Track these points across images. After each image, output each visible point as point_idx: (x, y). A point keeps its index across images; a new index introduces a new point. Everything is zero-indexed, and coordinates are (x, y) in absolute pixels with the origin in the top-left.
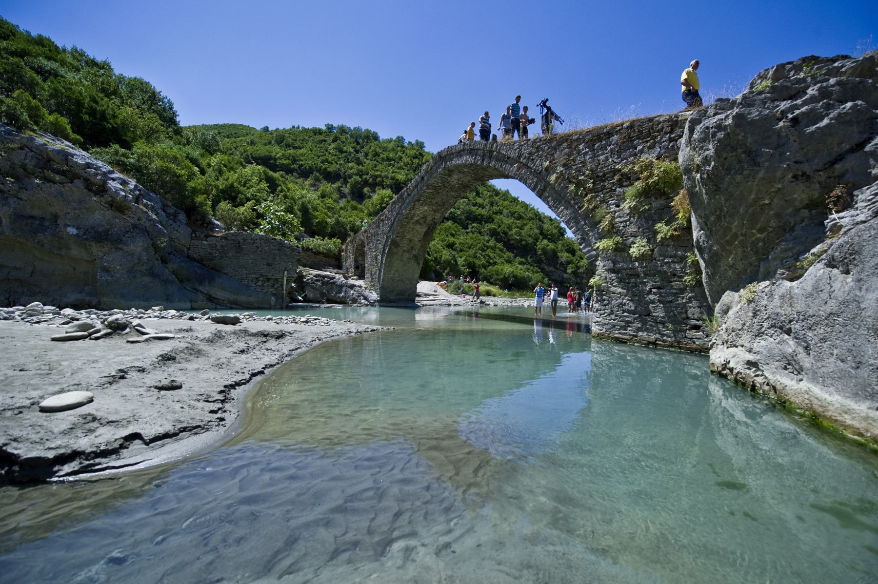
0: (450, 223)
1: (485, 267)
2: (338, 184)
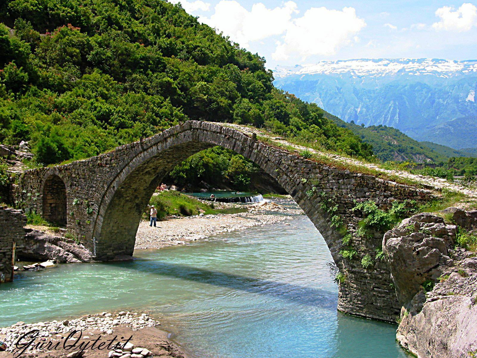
0: (96, 74)
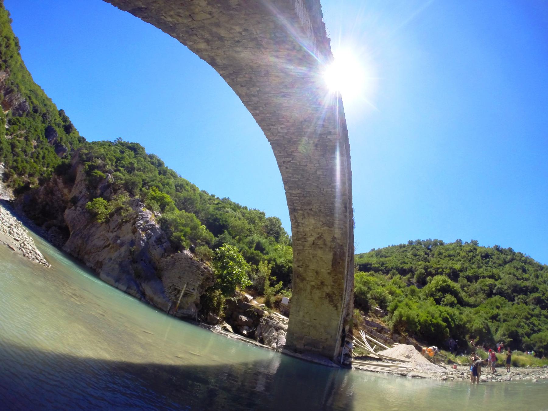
1: (528, 335)
2: (408, 276)
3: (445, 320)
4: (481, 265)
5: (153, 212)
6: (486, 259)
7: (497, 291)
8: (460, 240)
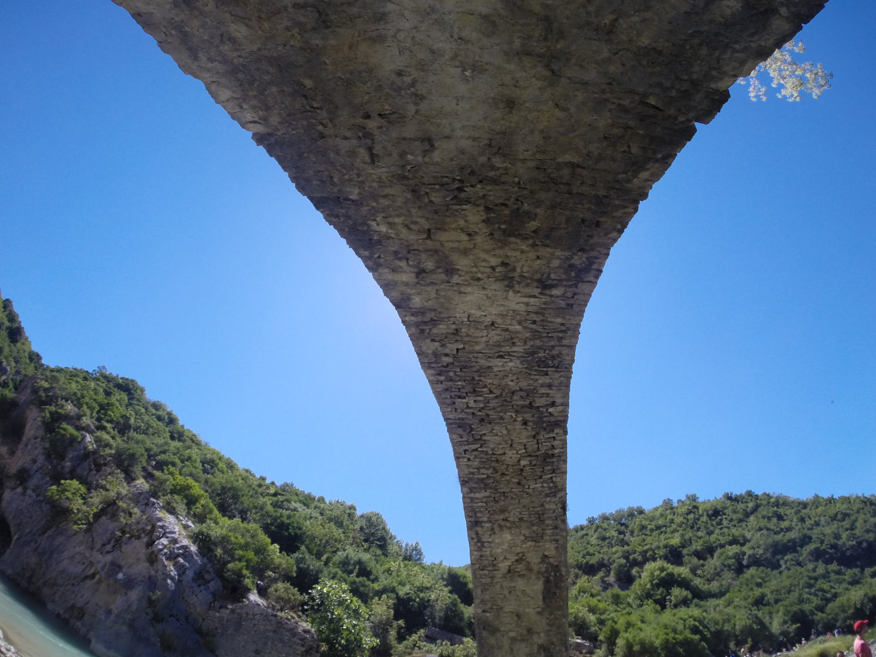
2: (601, 574)
3: (695, 630)
4: (712, 528)
5: (177, 518)
6: (716, 518)
7: (748, 561)
8: (669, 499)
